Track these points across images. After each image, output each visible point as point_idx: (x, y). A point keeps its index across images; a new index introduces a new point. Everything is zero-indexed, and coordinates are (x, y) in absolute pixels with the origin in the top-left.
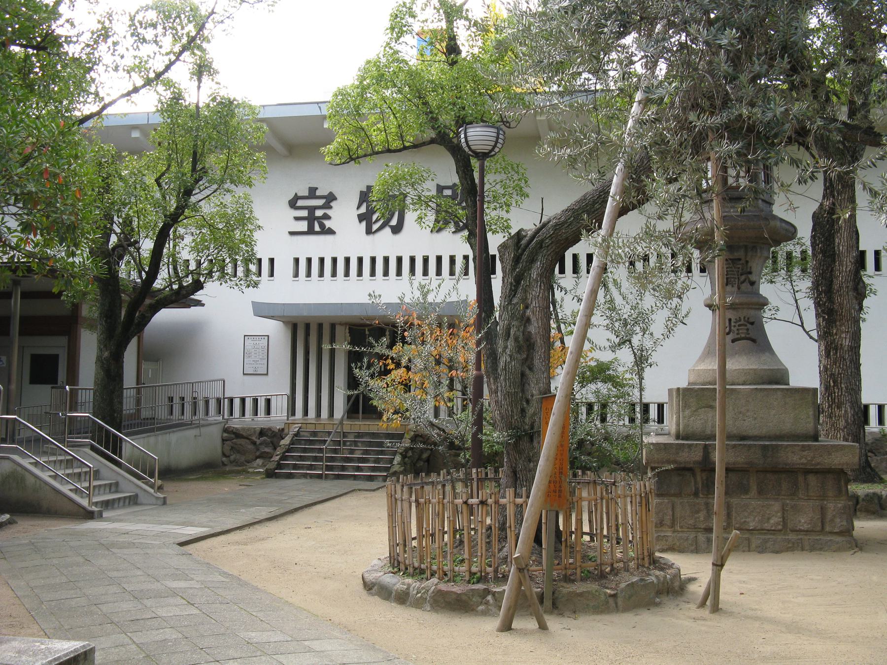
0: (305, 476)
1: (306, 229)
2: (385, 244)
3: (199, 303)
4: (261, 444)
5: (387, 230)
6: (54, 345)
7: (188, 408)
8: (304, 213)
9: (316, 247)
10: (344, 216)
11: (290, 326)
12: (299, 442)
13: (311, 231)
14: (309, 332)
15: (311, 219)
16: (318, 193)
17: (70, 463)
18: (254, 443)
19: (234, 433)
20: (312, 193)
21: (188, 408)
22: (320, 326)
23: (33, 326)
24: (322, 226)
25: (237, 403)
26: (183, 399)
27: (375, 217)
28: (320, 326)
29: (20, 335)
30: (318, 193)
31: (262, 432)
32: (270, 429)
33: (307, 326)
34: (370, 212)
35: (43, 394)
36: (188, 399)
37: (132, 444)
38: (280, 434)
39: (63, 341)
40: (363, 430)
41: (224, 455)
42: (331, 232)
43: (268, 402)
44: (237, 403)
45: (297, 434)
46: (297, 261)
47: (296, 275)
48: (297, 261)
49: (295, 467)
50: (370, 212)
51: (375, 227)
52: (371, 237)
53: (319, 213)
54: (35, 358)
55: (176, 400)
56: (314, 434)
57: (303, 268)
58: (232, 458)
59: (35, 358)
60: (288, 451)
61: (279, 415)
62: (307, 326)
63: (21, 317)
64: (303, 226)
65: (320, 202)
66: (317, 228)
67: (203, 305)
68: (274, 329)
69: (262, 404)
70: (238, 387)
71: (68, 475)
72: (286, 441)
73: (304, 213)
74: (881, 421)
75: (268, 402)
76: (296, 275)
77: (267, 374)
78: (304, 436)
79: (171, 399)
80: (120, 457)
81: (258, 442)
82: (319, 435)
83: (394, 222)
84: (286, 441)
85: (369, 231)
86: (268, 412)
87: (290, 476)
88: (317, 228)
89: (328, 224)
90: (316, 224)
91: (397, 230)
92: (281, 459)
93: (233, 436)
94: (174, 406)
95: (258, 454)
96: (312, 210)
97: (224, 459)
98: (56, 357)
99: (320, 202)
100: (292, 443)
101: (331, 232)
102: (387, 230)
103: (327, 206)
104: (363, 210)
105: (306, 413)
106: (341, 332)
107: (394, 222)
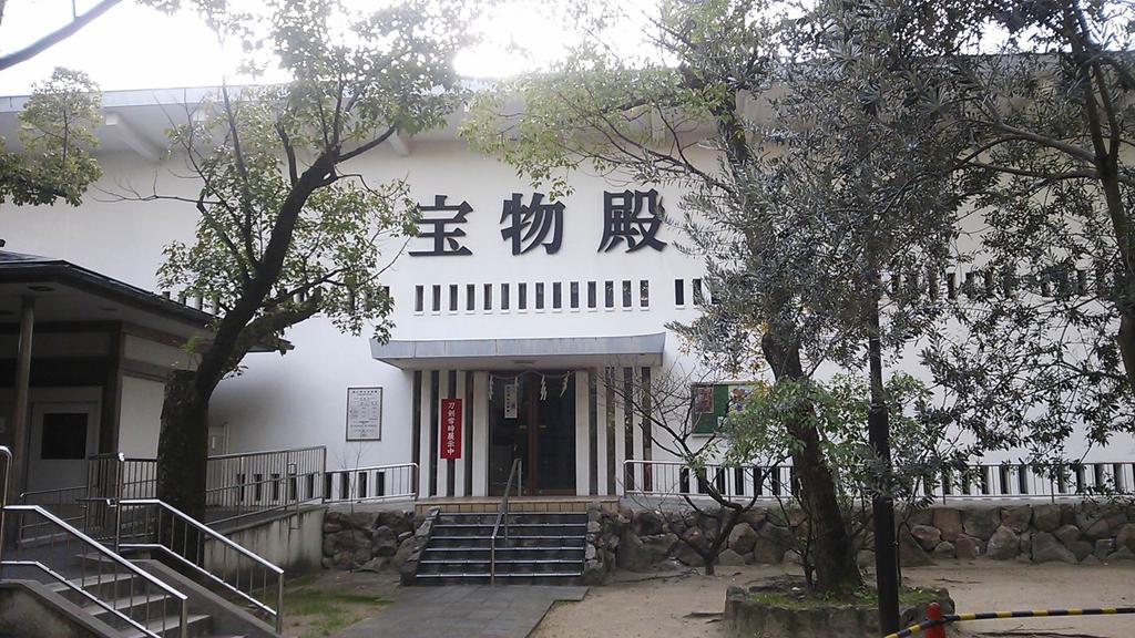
0: (460, 581)
1: (432, 249)
2: (537, 267)
3: (284, 347)
4: (379, 536)
5: (541, 250)
6: (81, 400)
7: (267, 489)
8: (431, 228)
9: (447, 271)
10: (484, 230)
11: (412, 374)
12: (440, 531)
13: (439, 251)
14: (441, 386)
15: (439, 236)
16: (447, 203)
17: (124, 590)
18: (369, 535)
19: (337, 521)
20: (440, 203)
21: (267, 489)
22: (453, 374)
23: (49, 373)
24: (454, 244)
25: (337, 480)
26: (259, 477)
27: (524, 233)
28: (453, 374)
29: (30, 385)
30: (447, 203)
31: (382, 519)
32: (393, 514)
33: (435, 375)
34: (518, 226)
35: (72, 474)
36: (267, 477)
37: (227, 546)
38: (408, 522)
39: (95, 393)
40: (529, 510)
41: (325, 553)
42: (465, 252)
43: (381, 476)
44: (337, 480)
45: (437, 520)
46: (420, 289)
47: (420, 307)
48: (420, 289)
49: (444, 568)
50: (518, 226)
51: (524, 246)
52: (519, 257)
53: (449, 228)
54: (50, 420)
55: (250, 479)
56: (461, 518)
57: (429, 298)
58: (337, 557)
59: (50, 420)
60: (431, 543)
61: (398, 495)
62: (435, 375)
63: (34, 361)
64: (428, 245)
65: (452, 214)
66: (447, 247)
67: (470, 253)
68: (393, 382)
69: (354, 479)
70: (345, 458)
71: (91, 589)
72: (423, 530)
73: (431, 228)
74: (381, 492)
75: (381, 476)
76: (420, 307)
77: (380, 440)
78: (446, 522)
79: (241, 478)
80: (201, 565)
81: (375, 532)
82: (468, 519)
83: (549, 239)
84: (423, 530)
85: (516, 251)
86: (381, 492)
87: (440, 582)
88: (447, 247)
89: (461, 242)
90: (446, 242)
91: (553, 249)
92: (422, 557)
93: (338, 526)
94: (264, 486)
95: (375, 550)
96: (439, 224)
97: (325, 560)
98: (85, 416)
99: (452, 214)
100: (433, 532)
101: (465, 252)
102: (541, 250)
103: (460, 219)
104: (509, 223)
105: (433, 490)
106: (480, 382)
107: (549, 239)
